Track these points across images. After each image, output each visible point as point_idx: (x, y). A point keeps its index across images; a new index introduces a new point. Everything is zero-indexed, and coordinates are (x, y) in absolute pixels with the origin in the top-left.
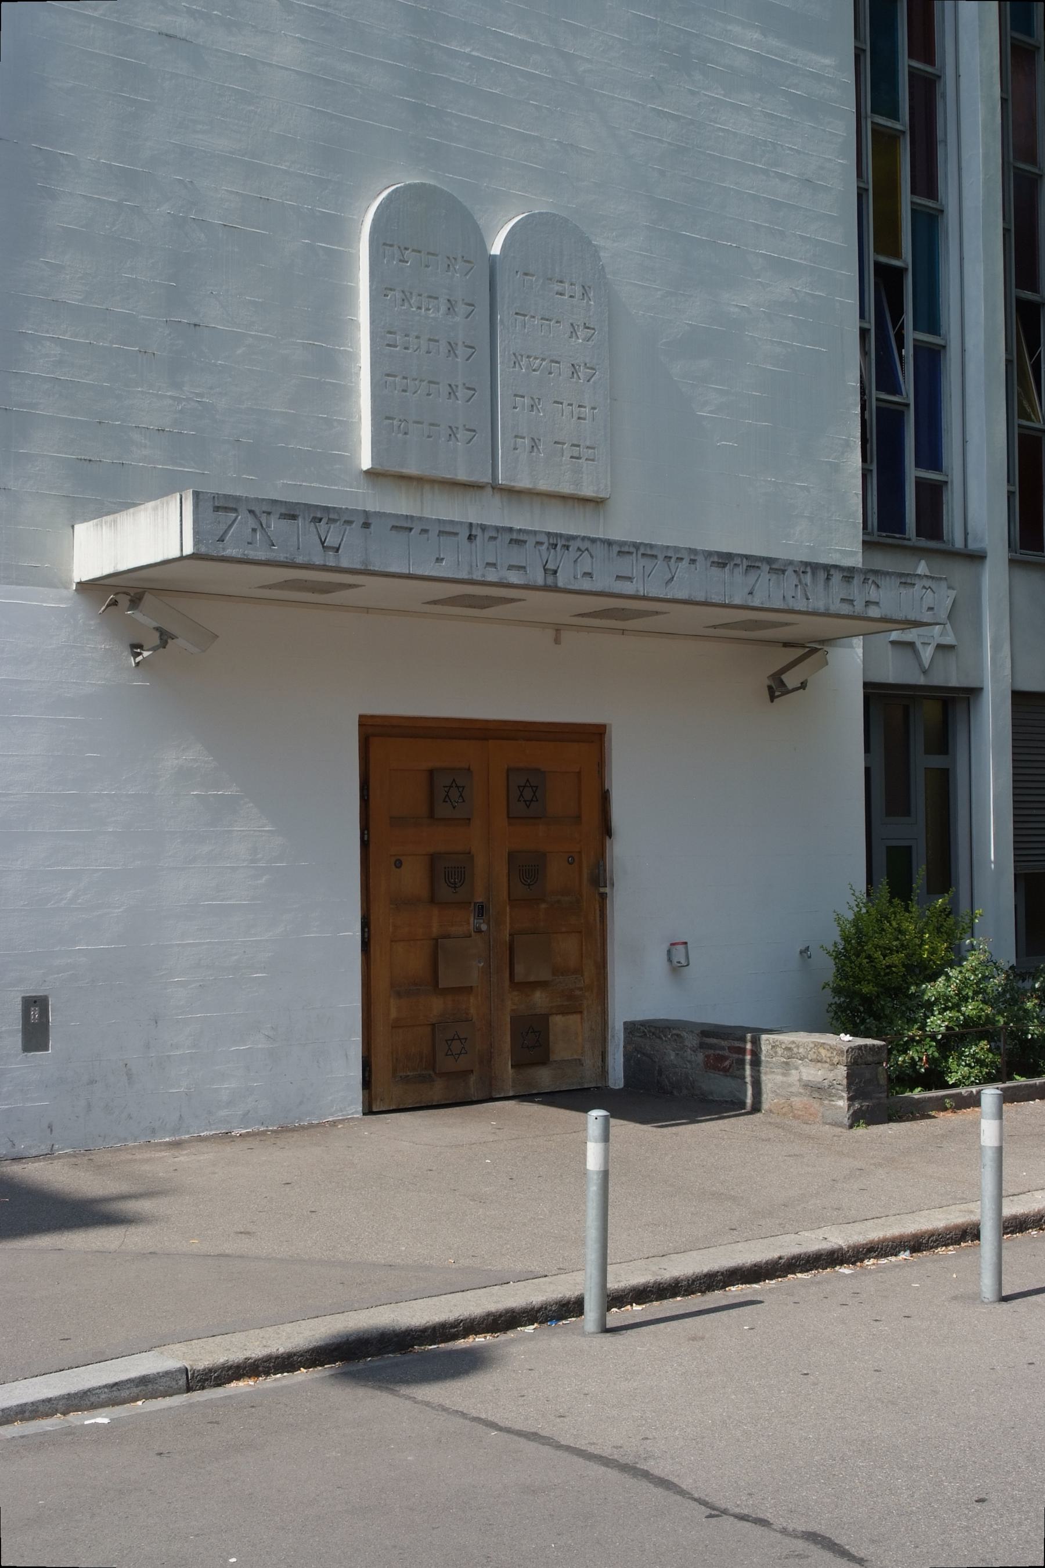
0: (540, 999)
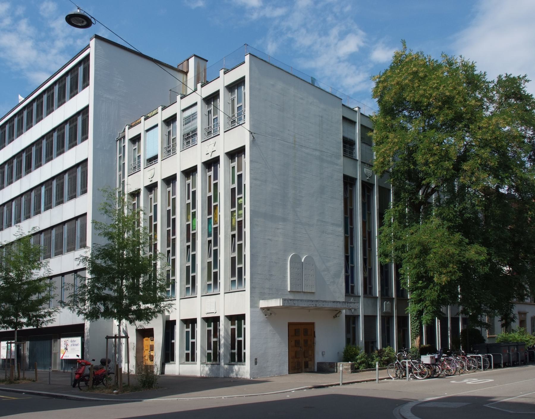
0: (307, 359)
